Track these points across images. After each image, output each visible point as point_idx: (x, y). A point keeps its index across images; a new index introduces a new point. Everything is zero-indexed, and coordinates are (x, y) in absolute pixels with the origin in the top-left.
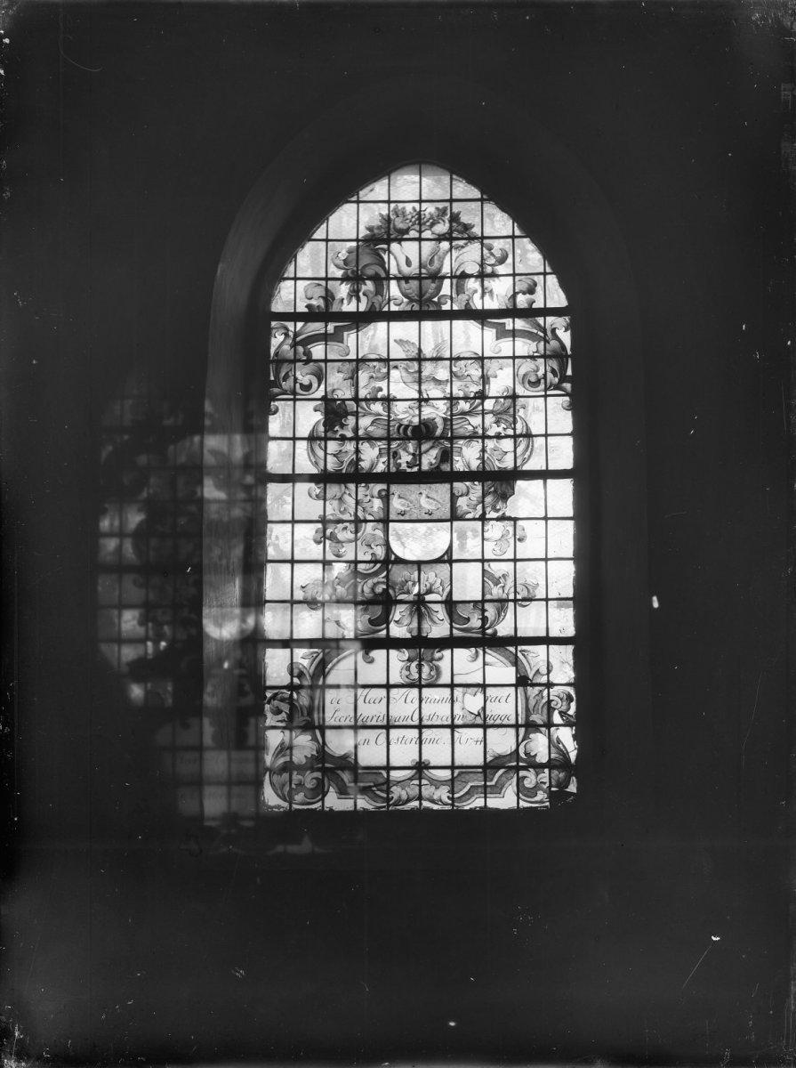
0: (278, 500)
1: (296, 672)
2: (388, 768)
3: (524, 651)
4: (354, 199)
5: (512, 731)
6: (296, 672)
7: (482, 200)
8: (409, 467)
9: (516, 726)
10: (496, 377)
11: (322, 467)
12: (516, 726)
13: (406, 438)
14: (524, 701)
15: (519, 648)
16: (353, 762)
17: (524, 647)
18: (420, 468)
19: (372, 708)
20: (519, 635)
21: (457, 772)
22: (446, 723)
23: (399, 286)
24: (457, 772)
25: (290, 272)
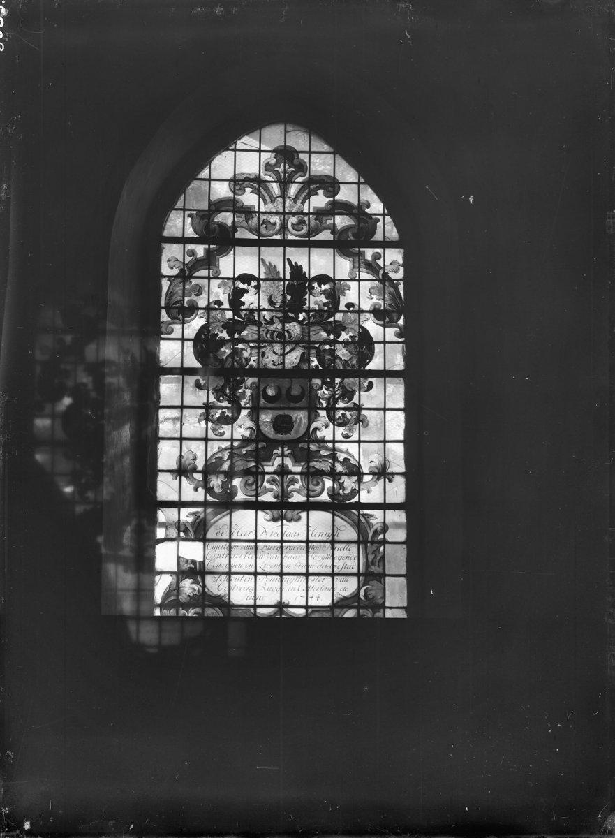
0: (168, 389)
1: (182, 528)
2: (255, 606)
3: (366, 515)
4: (233, 147)
5: (355, 579)
6: (182, 528)
7: (334, 153)
8: (274, 365)
9: (358, 575)
10: (368, 492)
11: (298, 477)
12: (358, 575)
13: (272, 342)
14: (365, 555)
15: (361, 512)
16: (227, 601)
17: (366, 512)
18: (284, 366)
19: (319, 561)
20: (307, 249)
21: (310, 610)
22: (235, 576)
23: (384, 597)
24: (310, 610)
25: (180, 204)
